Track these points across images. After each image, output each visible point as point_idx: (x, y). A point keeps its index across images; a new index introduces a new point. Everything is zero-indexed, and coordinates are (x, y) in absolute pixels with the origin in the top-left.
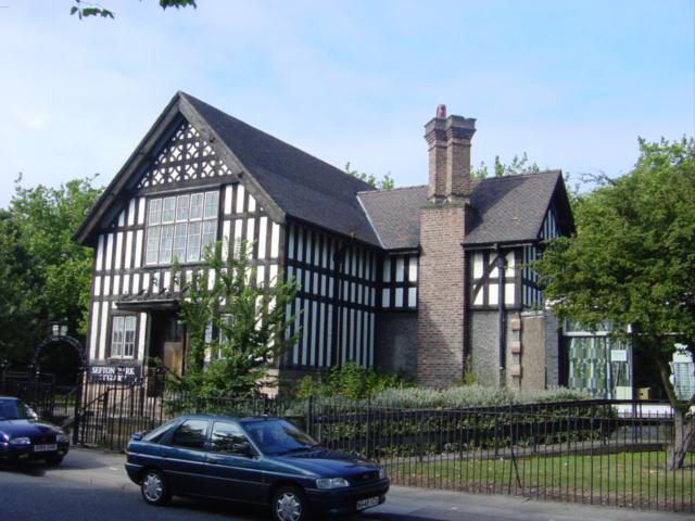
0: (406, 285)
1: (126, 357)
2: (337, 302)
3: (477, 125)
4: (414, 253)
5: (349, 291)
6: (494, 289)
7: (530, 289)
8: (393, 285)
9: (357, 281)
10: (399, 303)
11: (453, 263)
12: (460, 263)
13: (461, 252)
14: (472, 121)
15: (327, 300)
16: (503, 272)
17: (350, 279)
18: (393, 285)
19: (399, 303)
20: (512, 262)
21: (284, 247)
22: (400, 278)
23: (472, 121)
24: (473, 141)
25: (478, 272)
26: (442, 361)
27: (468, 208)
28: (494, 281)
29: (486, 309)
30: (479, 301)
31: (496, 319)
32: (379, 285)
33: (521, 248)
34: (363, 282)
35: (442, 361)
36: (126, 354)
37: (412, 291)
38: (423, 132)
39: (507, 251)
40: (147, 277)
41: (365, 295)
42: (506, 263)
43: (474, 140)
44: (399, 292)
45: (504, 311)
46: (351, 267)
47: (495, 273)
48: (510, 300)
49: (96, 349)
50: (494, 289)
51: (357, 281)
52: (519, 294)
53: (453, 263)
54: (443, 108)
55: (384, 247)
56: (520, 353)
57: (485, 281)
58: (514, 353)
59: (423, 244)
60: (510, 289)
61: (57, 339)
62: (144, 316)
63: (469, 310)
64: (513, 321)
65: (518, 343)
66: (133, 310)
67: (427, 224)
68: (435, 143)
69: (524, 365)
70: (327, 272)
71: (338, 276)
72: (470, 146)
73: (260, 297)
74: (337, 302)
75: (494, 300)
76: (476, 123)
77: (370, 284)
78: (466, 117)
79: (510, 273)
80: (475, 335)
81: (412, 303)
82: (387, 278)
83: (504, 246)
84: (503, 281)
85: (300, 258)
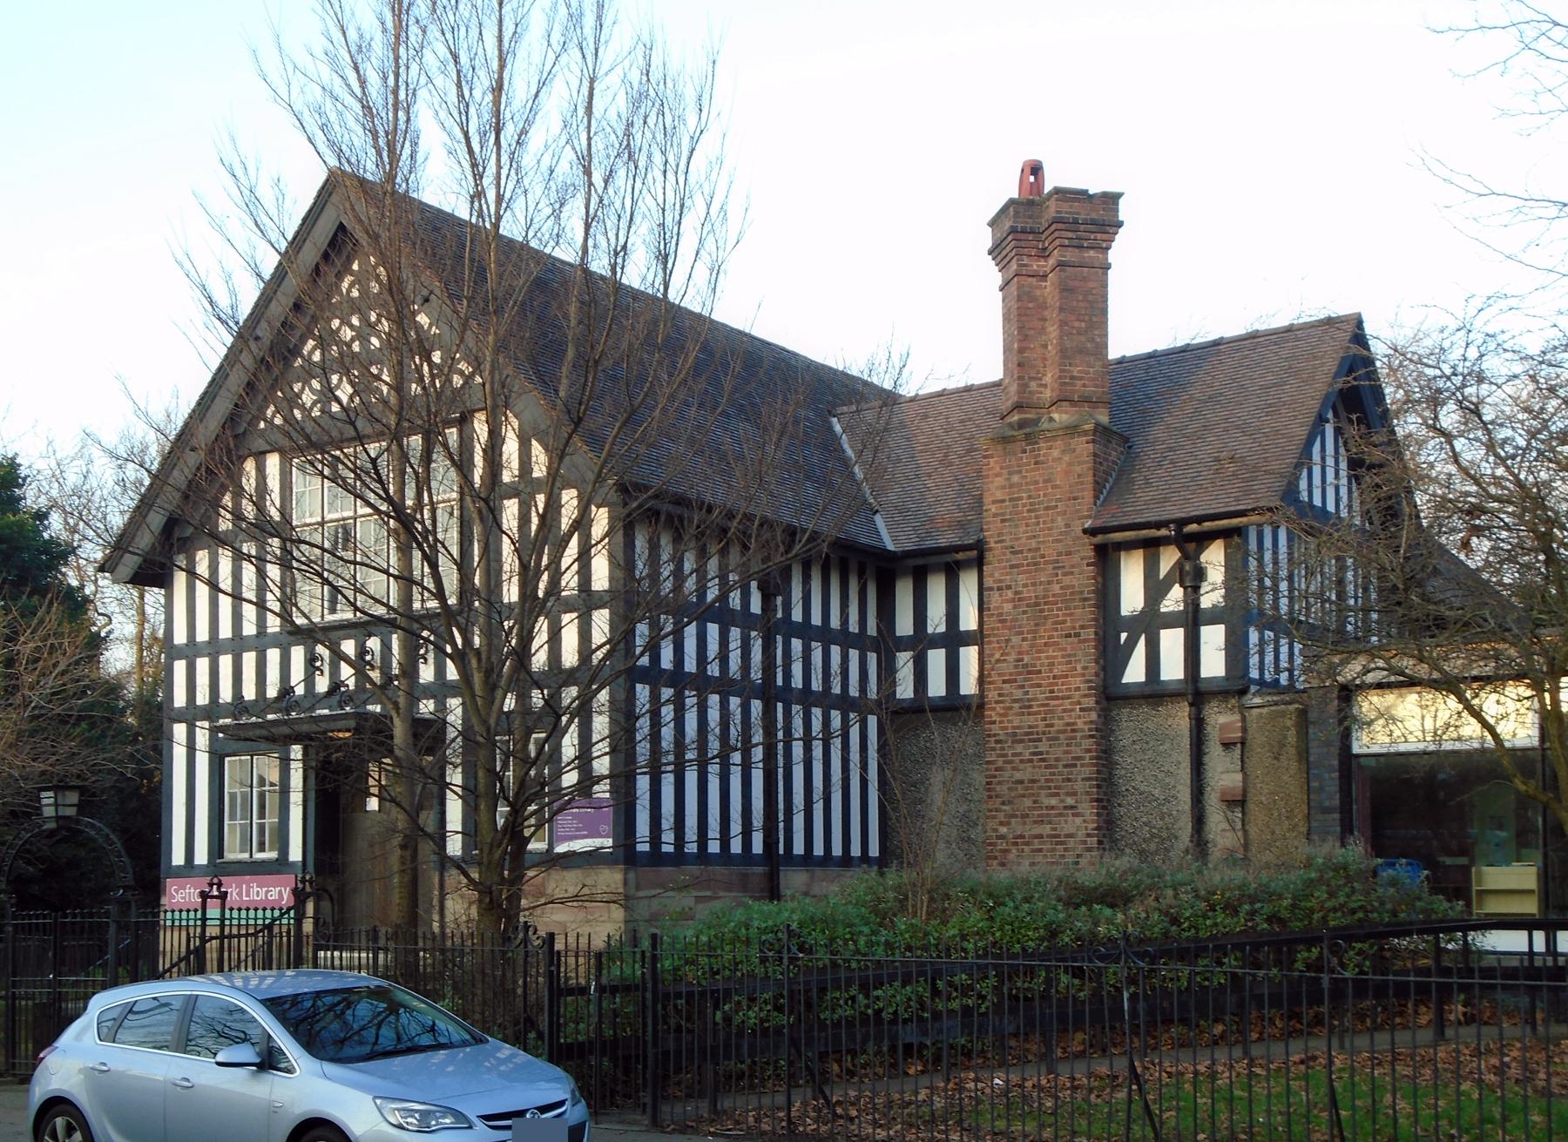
0: (954, 639)
1: (259, 856)
2: (770, 693)
3: (1124, 211)
4: (956, 559)
5: (803, 665)
6: (1172, 642)
7: (1317, 502)
8: (921, 642)
9: (826, 636)
10: (937, 687)
11: (1067, 580)
12: (1083, 577)
13: (1085, 550)
14: (1111, 200)
15: (745, 690)
16: (1193, 591)
17: (805, 631)
18: (921, 642)
19: (937, 687)
20: (1214, 558)
21: (623, 564)
22: (936, 620)
23: (1111, 200)
24: (1112, 256)
25: (1132, 598)
26: (1046, 829)
27: (1103, 433)
28: (1171, 621)
29: (1154, 693)
30: (1135, 672)
31: (1179, 717)
32: (886, 645)
33: (1239, 531)
34: (845, 639)
35: (1046, 829)
36: (262, 849)
37: (969, 657)
38: (986, 239)
39: (1204, 539)
40: (298, 654)
41: (855, 671)
42: (1200, 574)
43: (1120, 252)
44: (936, 659)
45: (1196, 691)
46: (810, 600)
47: (1174, 599)
48: (1213, 665)
49: (186, 834)
50: (1172, 642)
51: (826, 636)
52: (1236, 650)
53: (1067, 580)
54: (1035, 169)
55: (891, 547)
56: (1237, 802)
57: (1150, 623)
58: (1227, 745)
59: (991, 536)
60: (1213, 638)
61: (52, 825)
62: (296, 751)
63: (1112, 695)
64: (1221, 719)
65: (1239, 777)
66: (272, 739)
67: (999, 481)
68: (1014, 266)
69: (1253, 831)
70: (745, 620)
71: (772, 628)
72: (1108, 267)
73: (573, 691)
74: (770, 693)
75: (1172, 668)
76: (1121, 201)
77: (860, 641)
78: (1094, 189)
79: (1211, 598)
80: (1125, 761)
81: (968, 685)
82: (904, 625)
83: (1194, 527)
84: (1192, 620)
85: (816, 620)
